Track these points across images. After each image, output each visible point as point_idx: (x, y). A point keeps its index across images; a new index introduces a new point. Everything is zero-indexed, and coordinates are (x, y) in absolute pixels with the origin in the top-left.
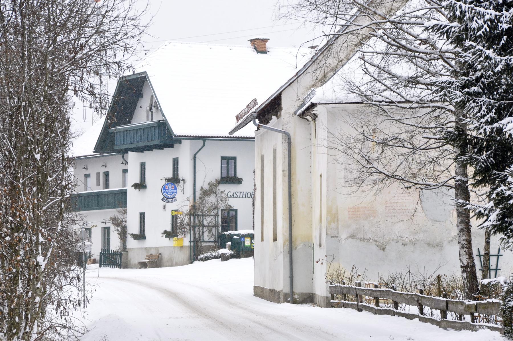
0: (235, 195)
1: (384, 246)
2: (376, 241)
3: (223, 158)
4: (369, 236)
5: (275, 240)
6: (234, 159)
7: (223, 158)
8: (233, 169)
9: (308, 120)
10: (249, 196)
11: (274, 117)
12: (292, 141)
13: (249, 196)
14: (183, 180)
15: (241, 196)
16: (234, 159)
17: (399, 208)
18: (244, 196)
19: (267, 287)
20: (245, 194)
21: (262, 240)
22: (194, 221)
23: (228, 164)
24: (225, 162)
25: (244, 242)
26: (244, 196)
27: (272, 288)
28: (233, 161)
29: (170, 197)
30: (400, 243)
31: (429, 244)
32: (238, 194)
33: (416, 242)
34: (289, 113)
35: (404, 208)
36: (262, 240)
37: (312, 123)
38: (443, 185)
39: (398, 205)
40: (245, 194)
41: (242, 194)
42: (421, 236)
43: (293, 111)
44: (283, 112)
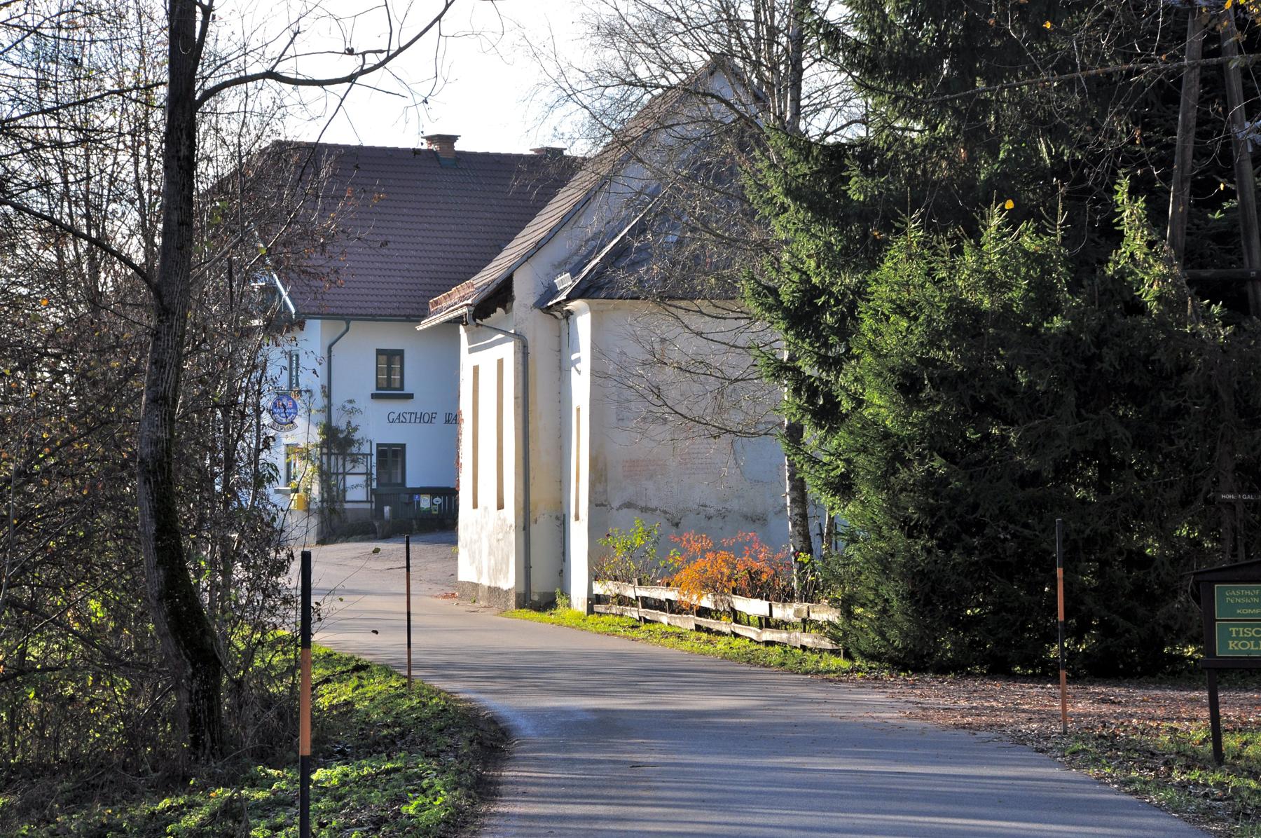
0: (402, 418)
1: (676, 520)
2: (665, 512)
3: (380, 352)
4: (653, 505)
5: (500, 506)
6: (400, 353)
7: (380, 352)
8: (398, 371)
9: (556, 317)
10: (426, 420)
11: (499, 310)
12: (530, 350)
13: (426, 420)
14: (308, 391)
15: (413, 420)
16: (400, 353)
17: (700, 461)
18: (418, 420)
19: (486, 582)
20: (418, 416)
21: (475, 506)
22: (329, 464)
23: (389, 363)
24: (383, 358)
25: (419, 502)
26: (418, 420)
27: (493, 585)
28: (397, 358)
29: (284, 420)
30: (702, 516)
31: (746, 517)
32: (408, 417)
33: (727, 514)
34: (525, 306)
35: (708, 461)
36: (475, 506)
37: (564, 322)
38: (766, 434)
39: (700, 456)
40: (418, 416)
41: (413, 416)
42: (735, 505)
43: (532, 300)
44: (515, 304)
